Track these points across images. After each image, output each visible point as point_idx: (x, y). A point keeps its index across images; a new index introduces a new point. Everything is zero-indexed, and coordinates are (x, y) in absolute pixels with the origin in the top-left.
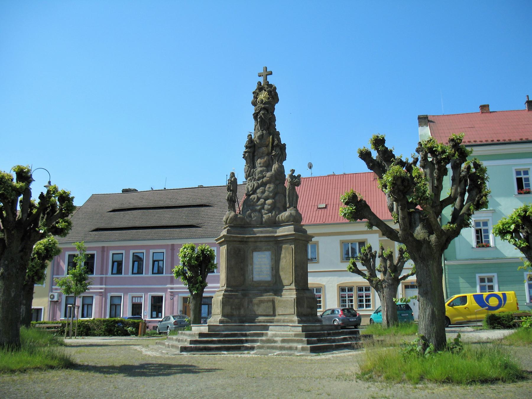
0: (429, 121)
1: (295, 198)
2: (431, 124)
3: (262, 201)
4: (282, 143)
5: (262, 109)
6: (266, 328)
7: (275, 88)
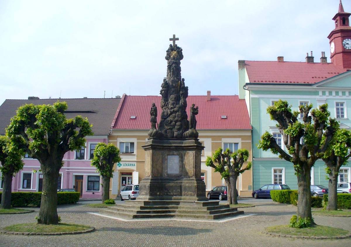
0: (245, 64)
1: (194, 123)
2: (247, 66)
3: (174, 123)
4: (186, 86)
5: (173, 63)
6: (178, 203)
7: (182, 50)
